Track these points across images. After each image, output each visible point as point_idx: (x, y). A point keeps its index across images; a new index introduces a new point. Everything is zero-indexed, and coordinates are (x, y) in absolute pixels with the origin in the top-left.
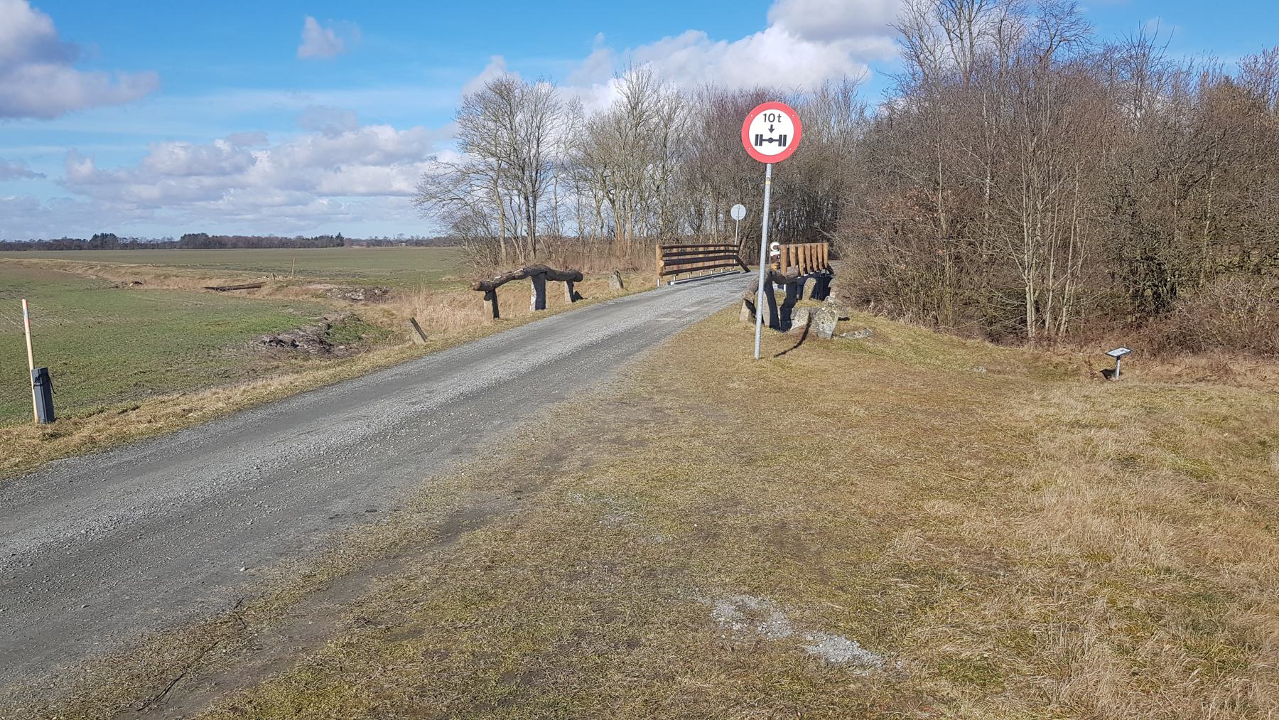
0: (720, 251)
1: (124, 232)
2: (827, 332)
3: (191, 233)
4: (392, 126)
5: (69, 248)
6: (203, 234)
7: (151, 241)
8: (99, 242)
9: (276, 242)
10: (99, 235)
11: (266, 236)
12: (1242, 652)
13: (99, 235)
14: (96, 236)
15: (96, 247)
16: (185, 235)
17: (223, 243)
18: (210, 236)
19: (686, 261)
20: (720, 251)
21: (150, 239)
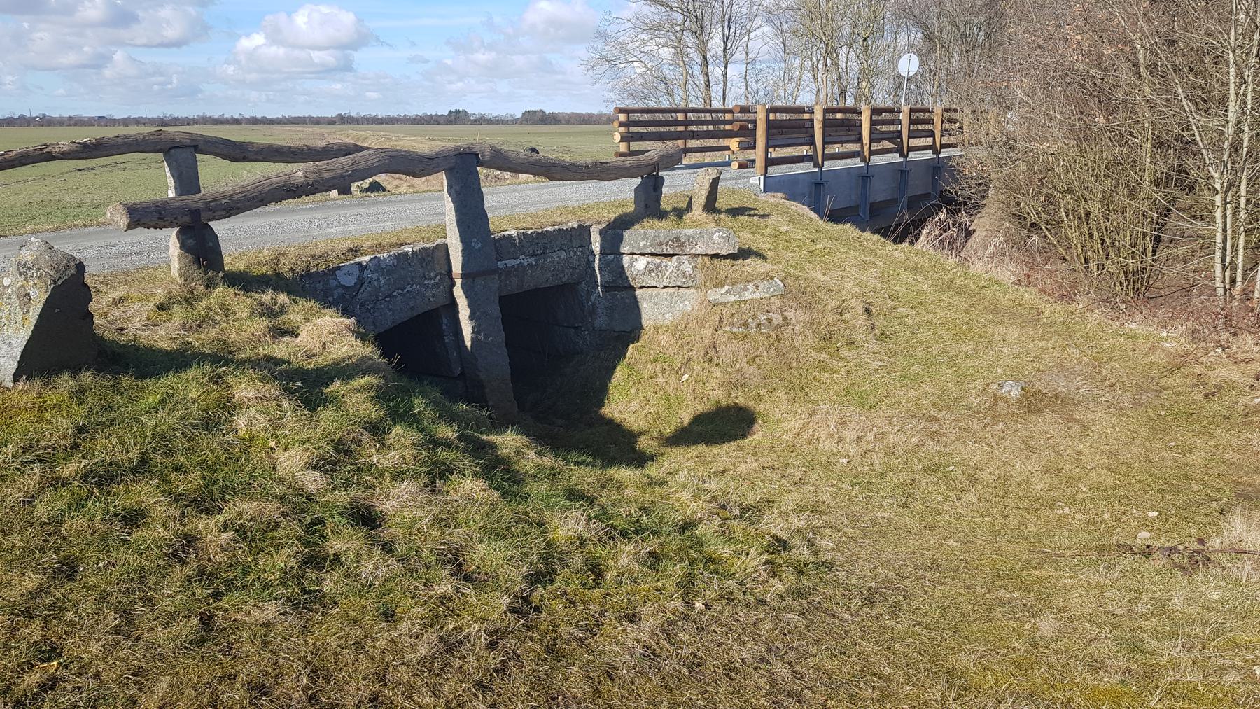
0: (677, 123)
1: (474, 109)
2: (972, 287)
3: (531, 110)
4: (296, 11)
5: (428, 123)
6: (541, 110)
7: (496, 117)
8: (453, 118)
9: (605, 119)
10: (454, 111)
11: (184, 116)
12: (234, 505)
13: (454, 111)
14: (451, 112)
15: (450, 122)
16: (526, 111)
17: (558, 119)
18: (287, 117)
19: (694, 135)
20: (677, 123)
21: (496, 115)
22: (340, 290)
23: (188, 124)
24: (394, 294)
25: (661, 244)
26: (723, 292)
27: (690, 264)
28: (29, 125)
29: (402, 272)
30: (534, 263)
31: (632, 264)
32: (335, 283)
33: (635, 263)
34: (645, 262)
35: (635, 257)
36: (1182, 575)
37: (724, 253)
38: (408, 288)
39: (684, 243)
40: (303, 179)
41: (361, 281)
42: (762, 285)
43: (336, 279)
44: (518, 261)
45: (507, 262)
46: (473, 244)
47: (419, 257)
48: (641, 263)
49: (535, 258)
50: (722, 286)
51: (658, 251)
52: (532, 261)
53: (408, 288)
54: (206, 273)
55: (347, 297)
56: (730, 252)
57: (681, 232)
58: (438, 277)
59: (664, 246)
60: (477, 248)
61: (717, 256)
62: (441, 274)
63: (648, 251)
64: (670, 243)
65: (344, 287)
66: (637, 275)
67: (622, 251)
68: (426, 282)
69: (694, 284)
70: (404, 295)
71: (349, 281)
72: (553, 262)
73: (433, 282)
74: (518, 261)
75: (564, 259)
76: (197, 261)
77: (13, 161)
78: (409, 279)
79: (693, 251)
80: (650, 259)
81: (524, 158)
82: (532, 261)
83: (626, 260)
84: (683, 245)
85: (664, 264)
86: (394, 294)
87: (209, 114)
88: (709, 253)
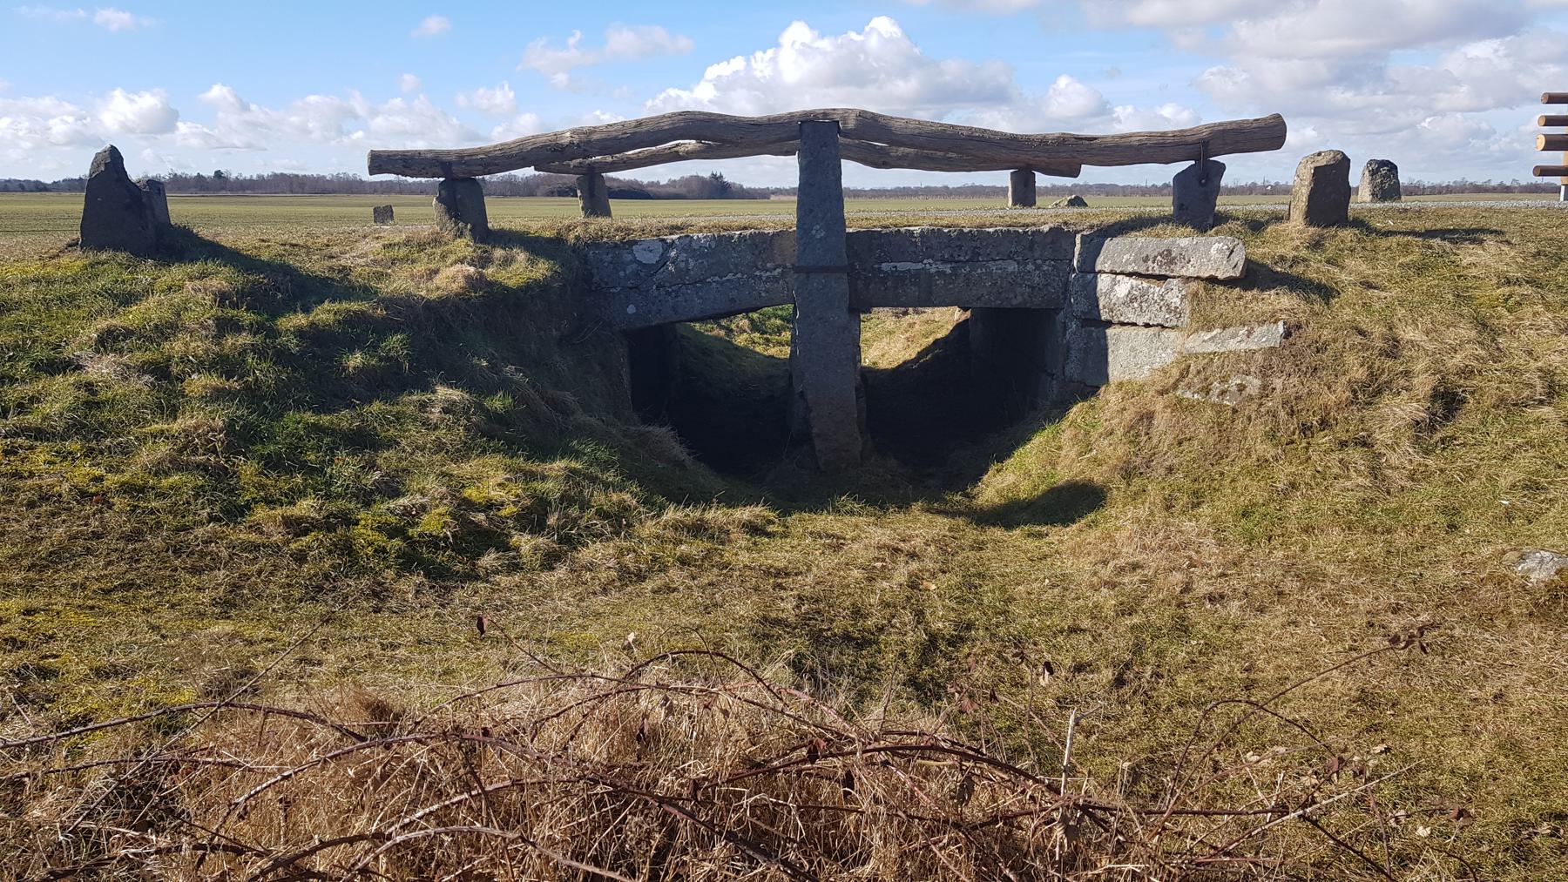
22: (634, 266)
23: (1440, 193)
24: (708, 280)
25: (1146, 260)
26: (1206, 338)
27: (1180, 291)
28: (1251, 193)
29: (722, 256)
30: (949, 271)
31: (1112, 289)
32: (630, 257)
33: (1116, 287)
34: (1129, 286)
35: (1119, 277)
36: (41, 487)
37: (1220, 276)
38: (730, 276)
39: (1175, 258)
40: (569, 139)
41: (664, 260)
42: (1258, 330)
43: (632, 252)
44: (920, 266)
45: (898, 265)
46: (814, 232)
47: (749, 242)
48: (1124, 286)
49: (953, 265)
50: (1210, 330)
51: (1142, 270)
52: (948, 269)
53: (730, 276)
54: (456, 224)
55: (642, 274)
56: (1228, 275)
57: (1174, 243)
58: (779, 270)
59: (1150, 263)
60: (818, 237)
61: (1212, 280)
62: (785, 267)
63: (1130, 269)
64: (1159, 258)
65: (640, 263)
66: (1115, 304)
67: (1098, 268)
68: (758, 273)
69: (1180, 324)
70: (722, 284)
71: (652, 258)
72: (990, 274)
73: (768, 274)
74: (920, 266)
75: (1012, 273)
76: (448, 211)
77: (645, 158)
78: (732, 267)
79: (1183, 272)
80: (1133, 281)
81: (915, 128)
82: (948, 269)
83: (1103, 282)
84: (1172, 261)
85: (1152, 290)
86: (708, 280)
87: (1470, 179)
88: (1201, 275)
